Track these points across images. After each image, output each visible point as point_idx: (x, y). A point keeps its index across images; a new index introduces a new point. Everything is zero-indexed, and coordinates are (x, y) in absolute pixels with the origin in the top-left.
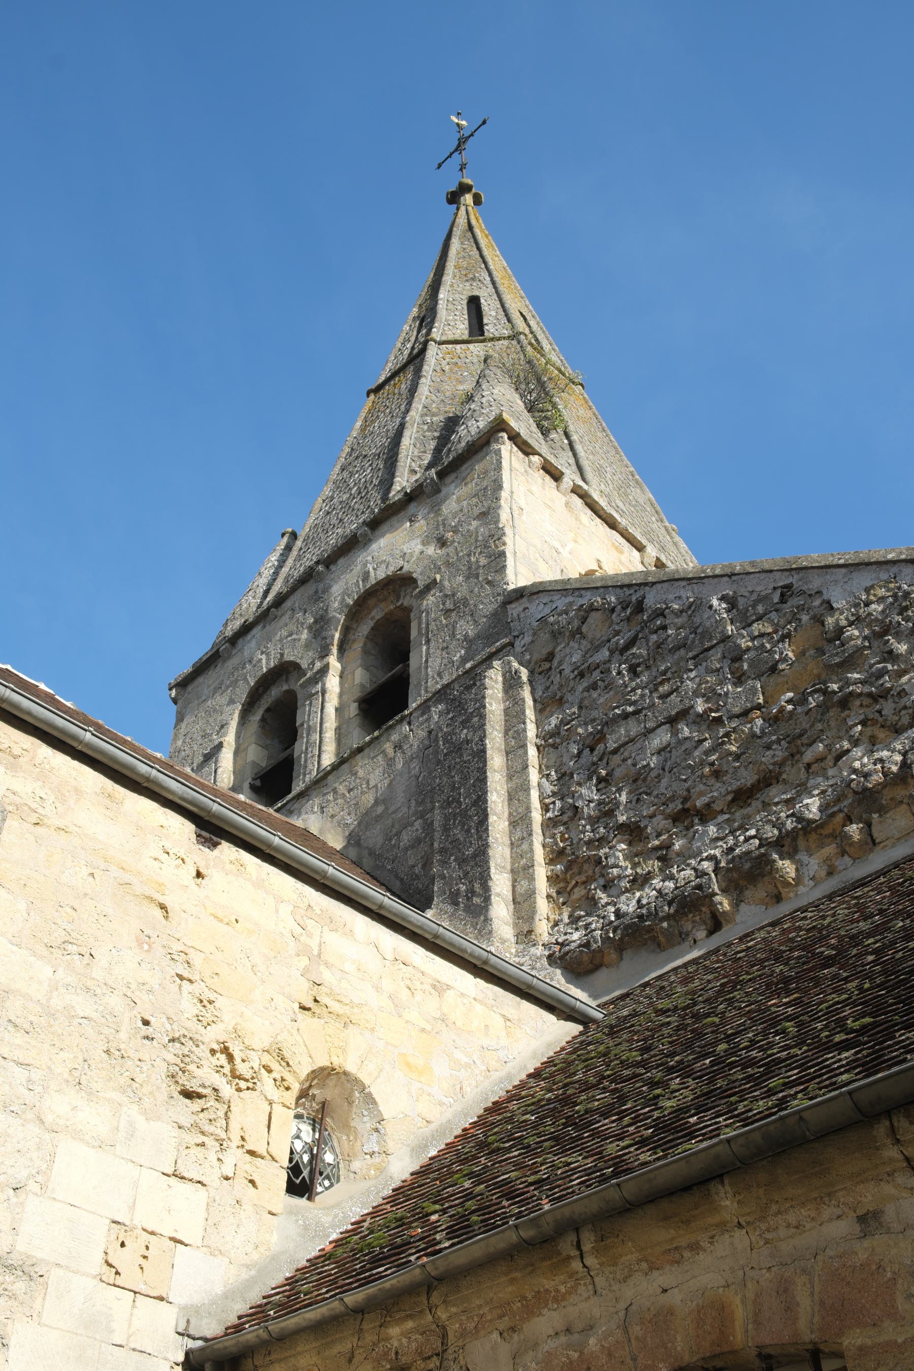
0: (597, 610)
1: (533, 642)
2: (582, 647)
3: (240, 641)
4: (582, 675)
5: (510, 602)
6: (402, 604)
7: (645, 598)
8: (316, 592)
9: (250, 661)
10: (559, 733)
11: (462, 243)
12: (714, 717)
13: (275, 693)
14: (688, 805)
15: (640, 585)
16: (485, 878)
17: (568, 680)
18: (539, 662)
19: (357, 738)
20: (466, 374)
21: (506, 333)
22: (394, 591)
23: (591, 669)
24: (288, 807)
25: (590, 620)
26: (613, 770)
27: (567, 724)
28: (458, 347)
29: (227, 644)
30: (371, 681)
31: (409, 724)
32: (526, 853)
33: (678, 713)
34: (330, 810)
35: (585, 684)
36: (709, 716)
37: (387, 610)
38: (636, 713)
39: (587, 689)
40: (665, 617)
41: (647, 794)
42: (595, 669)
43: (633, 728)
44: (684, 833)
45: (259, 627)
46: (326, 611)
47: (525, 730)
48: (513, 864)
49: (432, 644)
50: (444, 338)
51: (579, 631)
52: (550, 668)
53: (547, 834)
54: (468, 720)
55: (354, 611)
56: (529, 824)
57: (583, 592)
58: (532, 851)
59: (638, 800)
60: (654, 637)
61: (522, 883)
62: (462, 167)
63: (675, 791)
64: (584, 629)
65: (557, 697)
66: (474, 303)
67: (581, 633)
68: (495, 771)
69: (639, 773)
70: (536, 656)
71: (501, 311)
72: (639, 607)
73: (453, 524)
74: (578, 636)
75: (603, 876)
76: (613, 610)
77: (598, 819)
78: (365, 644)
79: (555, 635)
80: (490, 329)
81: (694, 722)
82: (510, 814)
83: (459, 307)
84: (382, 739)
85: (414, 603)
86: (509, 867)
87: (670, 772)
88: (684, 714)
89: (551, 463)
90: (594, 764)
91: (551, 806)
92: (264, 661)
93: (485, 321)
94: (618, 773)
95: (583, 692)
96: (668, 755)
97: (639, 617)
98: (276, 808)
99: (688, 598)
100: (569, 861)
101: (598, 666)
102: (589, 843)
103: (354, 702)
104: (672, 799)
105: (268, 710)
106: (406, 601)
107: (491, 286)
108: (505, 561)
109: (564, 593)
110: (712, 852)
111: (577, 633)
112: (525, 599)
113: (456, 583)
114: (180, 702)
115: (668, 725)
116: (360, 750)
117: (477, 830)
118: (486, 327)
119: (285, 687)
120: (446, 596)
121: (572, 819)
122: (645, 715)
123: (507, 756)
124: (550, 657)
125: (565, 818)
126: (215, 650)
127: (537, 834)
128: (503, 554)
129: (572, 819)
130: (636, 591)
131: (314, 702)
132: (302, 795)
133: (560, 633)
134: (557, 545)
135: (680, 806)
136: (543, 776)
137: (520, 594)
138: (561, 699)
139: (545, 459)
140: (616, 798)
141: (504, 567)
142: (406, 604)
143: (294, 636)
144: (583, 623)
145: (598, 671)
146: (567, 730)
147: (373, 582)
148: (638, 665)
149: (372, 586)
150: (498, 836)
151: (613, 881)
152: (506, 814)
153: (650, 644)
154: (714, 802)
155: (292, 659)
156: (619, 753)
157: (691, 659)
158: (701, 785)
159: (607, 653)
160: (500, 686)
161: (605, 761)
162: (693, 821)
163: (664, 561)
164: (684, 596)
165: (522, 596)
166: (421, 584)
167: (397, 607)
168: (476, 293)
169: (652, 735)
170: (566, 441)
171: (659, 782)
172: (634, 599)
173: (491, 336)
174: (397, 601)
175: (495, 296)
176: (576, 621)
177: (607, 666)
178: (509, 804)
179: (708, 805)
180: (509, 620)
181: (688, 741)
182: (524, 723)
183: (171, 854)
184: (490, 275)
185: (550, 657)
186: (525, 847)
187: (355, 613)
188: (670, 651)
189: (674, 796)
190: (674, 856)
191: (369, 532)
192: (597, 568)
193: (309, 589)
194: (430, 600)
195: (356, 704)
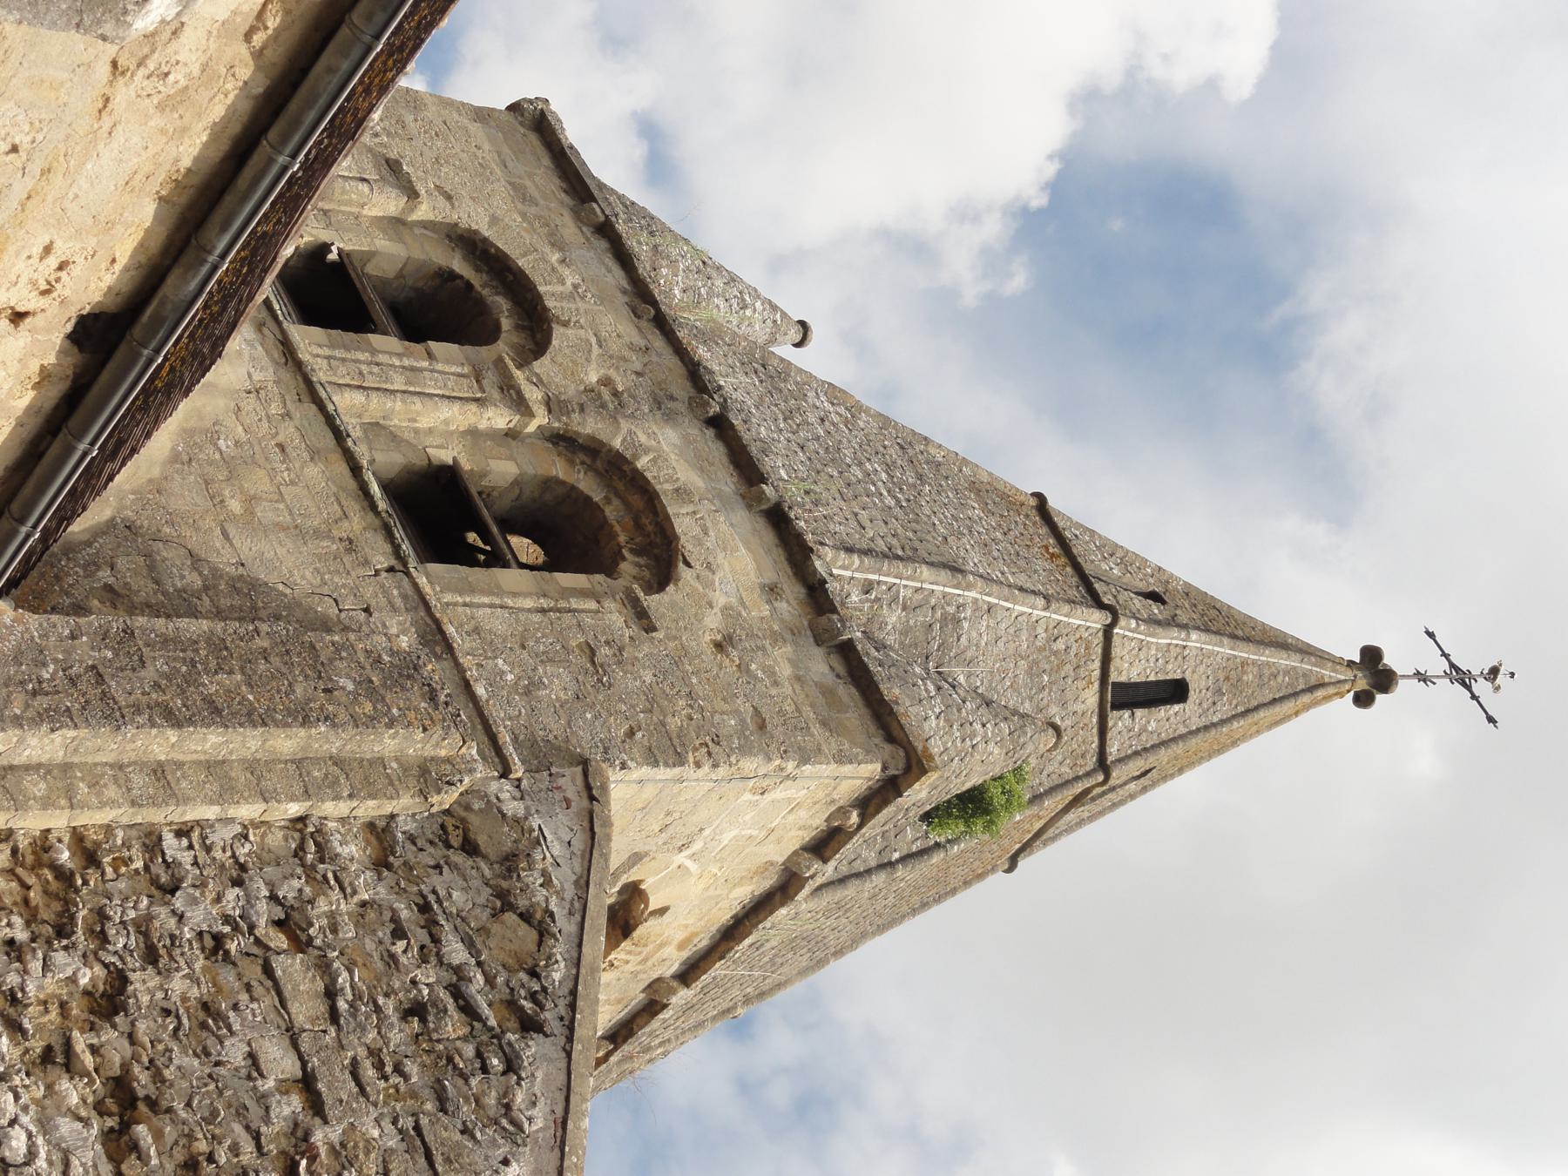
0: (540, 944)
1: (504, 815)
2: (478, 911)
3: (603, 244)
4: (425, 908)
5: (585, 774)
6: (624, 559)
7: (546, 1036)
8: (672, 398)
9: (563, 261)
10: (322, 861)
11: (1287, 673)
12: (297, 1164)
13: (502, 307)
14: (142, 1107)
15: (571, 1028)
16: (53, 718)
17: (417, 881)
18: (463, 825)
19: (380, 460)
20: (1046, 678)
21: (1113, 750)
22: (651, 543)
23: (431, 925)
24: (271, 323)
25: (524, 929)
26: (234, 964)
27: (336, 879)
28: (1097, 664)
29: (602, 218)
30: (494, 489)
31: (391, 570)
32: (99, 794)
33: (318, 1094)
34: (250, 403)
35: (404, 914)
36: (303, 1155)
37: (617, 528)
38: (334, 1016)
39: (395, 919)
40: (504, 1073)
41: (176, 1030)
42: (431, 935)
43: (307, 1009)
44: (90, 1100)
45: (625, 283)
46: (632, 416)
47: (337, 798)
48: (81, 766)
49: (537, 618)
50: (1116, 641)
51: (508, 906)
52: (448, 846)
53: (134, 833)
54: (372, 693)
55: (625, 468)
56: (154, 802)
57: (578, 917)
58: (102, 805)
59: (166, 1012)
60: (469, 1050)
61: (43, 785)
62: (1422, 677)
63: (171, 1085)
64: (510, 917)
65: (391, 859)
66: (1175, 691)
67: (502, 911)
68: (264, 741)
69: (219, 1016)
70: (474, 821)
71: (1155, 740)
72: (530, 1026)
73: (753, 667)
74: (499, 904)
75: (33, 940)
76: (534, 974)
77: (145, 934)
78: (563, 483)
79: (510, 862)
80: (1121, 721)
81: (296, 1125)
82: (180, 765)
83: (1170, 667)
84: (371, 515)
85: (621, 582)
86: (76, 760)
87: (210, 1076)
88: (316, 1105)
89: (846, 843)
90: (252, 927)
91: (185, 842)
92: (559, 288)
93: (1139, 712)
94: (228, 976)
95: (394, 911)
96: (244, 1072)
97: (512, 1024)
98: (272, 298)
99: (530, 1119)
100: (72, 874)
101: (436, 940)
102: (101, 915)
103: (454, 459)
104: (158, 1077)
105: (469, 286)
106: (627, 567)
107: (1203, 722)
108: (667, 765)
109: (582, 882)
110: (43, 1154)
111: (504, 901)
112: (585, 803)
113: (637, 679)
114: (510, 117)
115: (299, 1074)
116: (356, 470)
117: (158, 704)
118: (1127, 714)
119: (506, 324)
120: (621, 650)
121: (155, 882)
122: (325, 1031)
123: (293, 761)
124: (470, 848)
125: (158, 869)
126: (596, 193)
127: (134, 814)
128: (680, 760)
129: (155, 882)
130: (562, 1019)
131: (465, 381)
132: (287, 349)
133: (509, 870)
134: (697, 846)
135: (141, 1093)
136: (245, 827)
137: (593, 794)
138: (389, 867)
139: (851, 835)
140: (178, 969)
141: (656, 764)
142: (624, 566)
143: (596, 350)
144: (521, 915)
145: (427, 940)
146: (325, 877)
147: (671, 510)
148: (423, 1020)
149: (664, 507)
150: (139, 743)
151: (20, 959)
152: (181, 757)
153: (458, 1043)
154: (139, 1158)
155: (555, 342)
156: (263, 978)
157: (417, 1121)
158: (175, 1135)
159: (456, 962)
160: (429, 751)
161: (255, 950)
162: (110, 1115)
163: (661, 1016)
164: (535, 1112)
165: (592, 798)
166: (652, 602)
167: (620, 548)
168: (1193, 696)
169: (287, 1042)
170: (896, 855)
171: (196, 1055)
172: (547, 1015)
173: (1110, 724)
174: (631, 551)
175: (1182, 730)
176: (527, 903)
177: (433, 960)
178: (199, 763)
179: (135, 1147)
180: (554, 770)
181: (262, 1112)
182: (351, 796)
183: (60, 274)
184: (1223, 722)
185: (470, 848)
186: (112, 792)
187: (620, 469)
188: (439, 1081)
189: (163, 1081)
190: (49, 1080)
191: (764, 507)
192: (651, 909)
193: (680, 387)
194: (616, 618)
195: (450, 462)
